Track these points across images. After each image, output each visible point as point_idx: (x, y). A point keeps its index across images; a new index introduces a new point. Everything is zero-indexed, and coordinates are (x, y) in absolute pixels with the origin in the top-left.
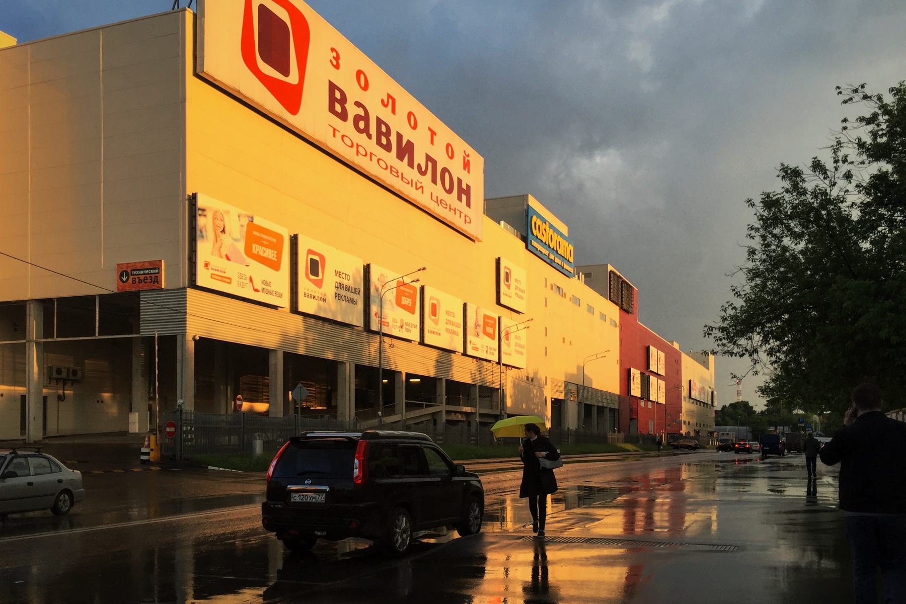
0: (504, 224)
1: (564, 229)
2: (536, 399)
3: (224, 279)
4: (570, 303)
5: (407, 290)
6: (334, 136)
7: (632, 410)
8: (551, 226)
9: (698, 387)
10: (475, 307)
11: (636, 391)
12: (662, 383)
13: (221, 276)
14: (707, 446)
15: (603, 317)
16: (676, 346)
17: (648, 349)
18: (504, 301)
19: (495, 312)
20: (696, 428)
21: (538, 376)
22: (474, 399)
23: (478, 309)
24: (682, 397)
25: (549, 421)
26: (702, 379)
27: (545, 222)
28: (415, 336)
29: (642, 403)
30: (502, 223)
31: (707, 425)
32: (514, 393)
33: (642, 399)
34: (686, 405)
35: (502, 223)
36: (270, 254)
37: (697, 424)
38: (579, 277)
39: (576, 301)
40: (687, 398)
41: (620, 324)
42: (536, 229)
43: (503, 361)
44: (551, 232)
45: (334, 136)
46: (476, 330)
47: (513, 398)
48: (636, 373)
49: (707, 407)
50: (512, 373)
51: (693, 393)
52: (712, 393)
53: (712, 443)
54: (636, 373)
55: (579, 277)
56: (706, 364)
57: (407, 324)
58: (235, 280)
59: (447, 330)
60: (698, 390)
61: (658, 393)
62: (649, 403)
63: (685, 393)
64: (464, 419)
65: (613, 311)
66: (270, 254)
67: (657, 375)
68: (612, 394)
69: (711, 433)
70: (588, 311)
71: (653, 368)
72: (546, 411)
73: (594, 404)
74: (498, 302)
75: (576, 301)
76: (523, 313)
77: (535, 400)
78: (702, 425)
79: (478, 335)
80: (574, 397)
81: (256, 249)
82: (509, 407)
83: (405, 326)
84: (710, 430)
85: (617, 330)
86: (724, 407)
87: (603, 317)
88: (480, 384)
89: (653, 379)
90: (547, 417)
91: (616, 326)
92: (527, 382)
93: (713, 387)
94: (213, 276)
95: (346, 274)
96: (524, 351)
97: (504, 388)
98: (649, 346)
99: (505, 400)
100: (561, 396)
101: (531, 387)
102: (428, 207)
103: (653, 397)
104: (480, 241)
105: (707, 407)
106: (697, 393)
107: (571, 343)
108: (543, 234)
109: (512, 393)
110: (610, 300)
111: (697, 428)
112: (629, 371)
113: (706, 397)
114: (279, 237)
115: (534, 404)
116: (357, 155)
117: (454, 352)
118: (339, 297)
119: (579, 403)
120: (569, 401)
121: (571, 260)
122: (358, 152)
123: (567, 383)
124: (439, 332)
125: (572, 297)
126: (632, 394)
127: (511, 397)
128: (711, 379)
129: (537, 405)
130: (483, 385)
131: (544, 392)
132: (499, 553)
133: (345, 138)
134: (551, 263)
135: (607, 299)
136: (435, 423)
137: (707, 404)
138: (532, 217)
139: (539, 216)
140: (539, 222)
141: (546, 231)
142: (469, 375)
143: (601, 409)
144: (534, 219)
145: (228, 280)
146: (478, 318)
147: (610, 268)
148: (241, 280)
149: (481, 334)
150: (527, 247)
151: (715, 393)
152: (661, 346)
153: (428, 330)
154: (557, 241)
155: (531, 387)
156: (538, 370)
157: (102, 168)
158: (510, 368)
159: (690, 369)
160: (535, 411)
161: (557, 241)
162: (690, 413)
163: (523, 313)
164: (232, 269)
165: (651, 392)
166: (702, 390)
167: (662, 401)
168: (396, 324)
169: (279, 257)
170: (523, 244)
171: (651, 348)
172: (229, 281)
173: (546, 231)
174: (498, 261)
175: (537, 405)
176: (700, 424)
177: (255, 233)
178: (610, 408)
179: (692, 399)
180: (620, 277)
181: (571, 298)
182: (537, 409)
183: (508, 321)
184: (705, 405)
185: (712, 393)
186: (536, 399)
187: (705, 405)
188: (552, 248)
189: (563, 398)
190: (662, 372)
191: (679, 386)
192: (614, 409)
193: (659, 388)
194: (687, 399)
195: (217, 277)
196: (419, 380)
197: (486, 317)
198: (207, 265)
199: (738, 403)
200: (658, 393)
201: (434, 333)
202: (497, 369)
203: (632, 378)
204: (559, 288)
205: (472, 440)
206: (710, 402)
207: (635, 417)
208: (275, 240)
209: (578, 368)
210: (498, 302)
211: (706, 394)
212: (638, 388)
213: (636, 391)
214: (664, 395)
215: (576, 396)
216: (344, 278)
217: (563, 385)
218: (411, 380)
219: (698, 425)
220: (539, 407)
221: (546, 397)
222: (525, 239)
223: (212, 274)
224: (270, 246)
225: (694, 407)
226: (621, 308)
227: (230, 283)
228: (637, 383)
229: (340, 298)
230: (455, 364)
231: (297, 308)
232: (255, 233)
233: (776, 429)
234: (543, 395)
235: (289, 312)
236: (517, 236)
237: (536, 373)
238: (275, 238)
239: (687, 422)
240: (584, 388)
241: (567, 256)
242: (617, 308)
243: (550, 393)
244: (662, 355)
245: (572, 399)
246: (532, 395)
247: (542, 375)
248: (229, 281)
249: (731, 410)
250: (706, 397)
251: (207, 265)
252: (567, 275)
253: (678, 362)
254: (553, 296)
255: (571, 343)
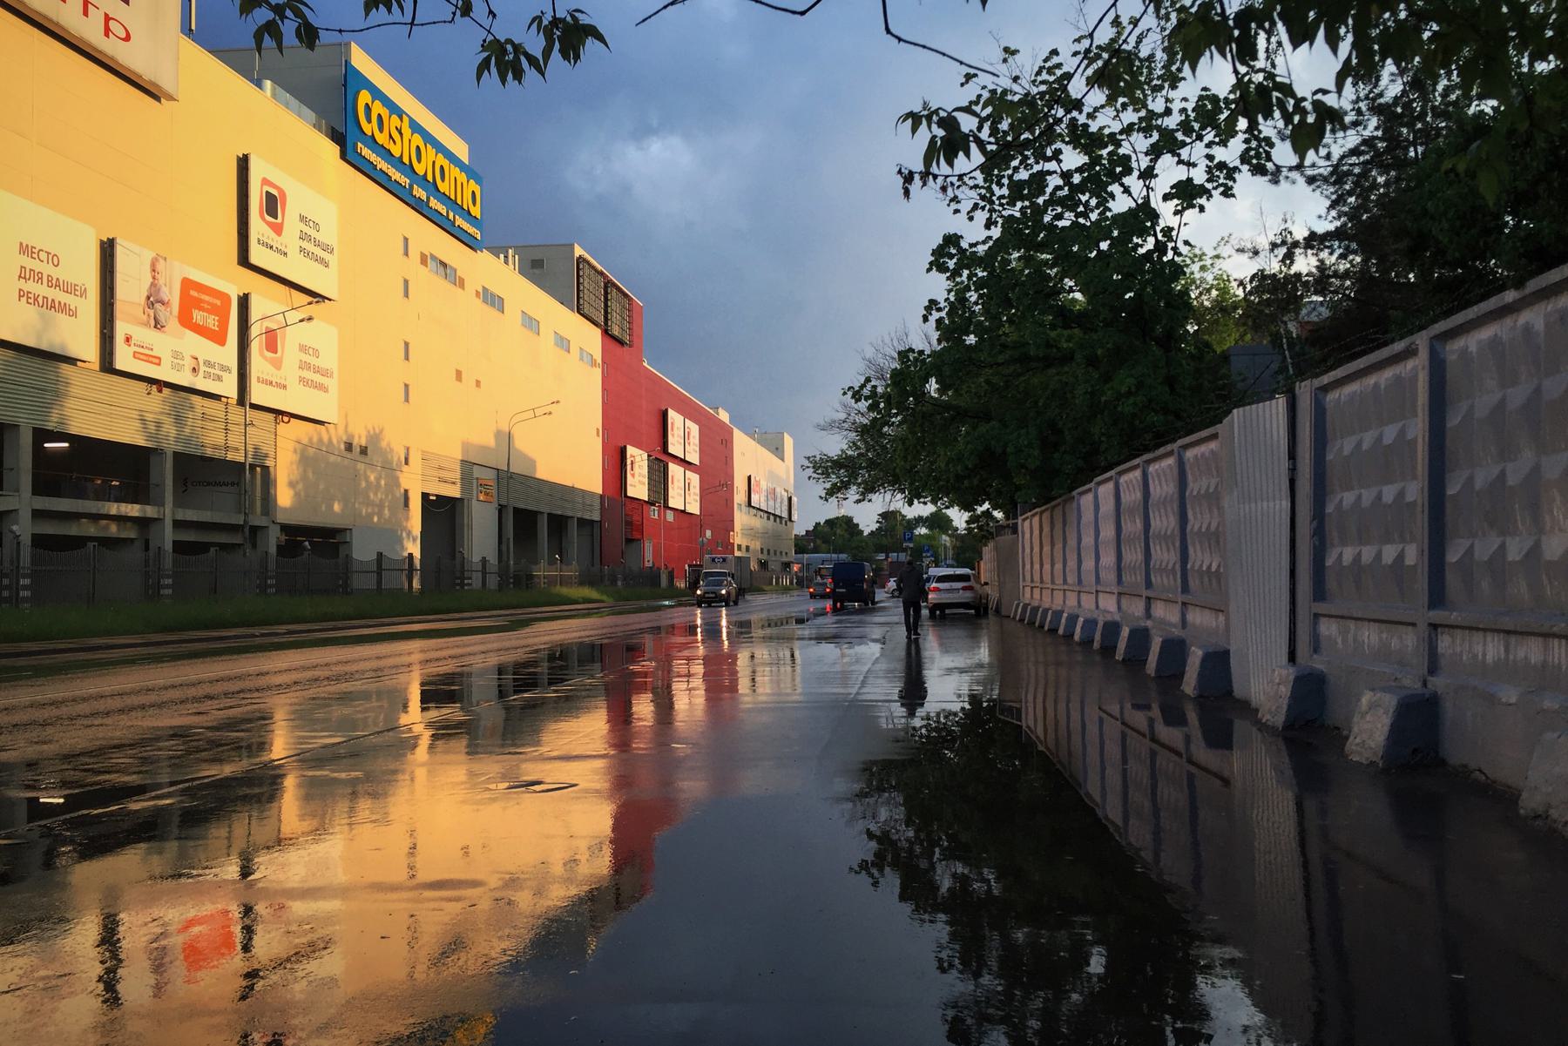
0: (273, 90)
1: (461, 149)
2: (376, 494)
3: (151, 359)
4: (479, 302)
5: (207, 298)
6: (86, 13)
7: (629, 524)
8: (416, 127)
9: (764, 488)
10: (149, 255)
11: (638, 487)
12: (694, 479)
13: (147, 355)
14: (766, 588)
15: (563, 343)
16: (724, 416)
17: (665, 415)
18: (257, 256)
19: (233, 283)
20: (760, 556)
21: (384, 444)
22: (160, 486)
23: (160, 266)
24: (736, 506)
25: (414, 540)
26: (772, 476)
27: (400, 114)
28: (229, 388)
29: (654, 513)
30: (268, 84)
31: (781, 553)
32: (304, 478)
33: (651, 503)
34: (742, 519)
35: (268, 84)
36: (212, 322)
37: (762, 549)
38: (506, 257)
39: (493, 300)
40: (743, 507)
41: (603, 362)
42: (369, 121)
43: (258, 395)
44: (417, 140)
45: (86, 13)
46: (151, 312)
47: (300, 486)
48: (638, 458)
49: (781, 523)
50: (291, 433)
51: (754, 497)
52: (790, 499)
53: (777, 583)
54: (638, 458)
55: (506, 257)
56: (778, 451)
57: (208, 363)
58: (167, 360)
59: (302, 380)
60: (764, 493)
61: (685, 493)
62: (668, 512)
63: (739, 497)
64: (133, 535)
65: (591, 338)
66: (212, 322)
67: (684, 462)
68: (593, 494)
69: (787, 565)
70: (524, 325)
71: (675, 448)
72: (407, 519)
73: (542, 510)
74: (244, 260)
75: (493, 300)
76: (330, 300)
77: (372, 495)
78: (772, 552)
79: (158, 325)
80: (487, 494)
81: (198, 316)
82: (285, 509)
83: (203, 368)
84: (785, 559)
85: (598, 373)
86: (818, 524)
87: (563, 343)
88: (180, 448)
89: (675, 470)
90: (409, 533)
91: (593, 363)
92: (348, 455)
93: (791, 490)
94: (137, 355)
95: (48, 253)
96: (332, 383)
97: (269, 463)
98: (667, 410)
99: (272, 491)
100: (454, 491)
101: (361, 466)
102: (55, 19)
103: (675, 501)
104: (171, 98)
105: (781, 523)
106: (763, 499)
107: (478, 383)
108: (391, 137)
109: (296, 476)
110: (578, 312)
111: (764, 557)
112: (623, 453)
113: (778, 505)
114: (225, 297)
115: (369, 503)
116: (107, 35)
117: (72, 361)
118: (28, 298)
119: (501, 509)
120: (474, 502)
121: (476, 211)
122: (107, 31)
123: (467, 466)
124: (283, 382)
125: (481, 290)
126: (629, 494)
127: (292, 485)
128: (788, 477)
129: (381, 506)
130: (192, 451)
131: (401, 480)
132: (578, 718)
133: (124, 36)
134: (419, 207)
135: (573, 310)
136: (147, 548)
137: (781, 517)
138: (357, 93)
139: (377, 94)
140: (378, 108)
141: (401, 134)
142: (138, 424)
143: (559, 523)
144: (364, 97)
145: (157, 361)
146: (161, 281)
147: (578, 251)
148: (176, 361)
149: (173, 324)
150: (343, 156)
151: (794, 499)
152: (690, 411)
153: (258, 378)
154: (434, 162)
155: (361, 466)
156: (381, 431)
157: (1039, 615)
158: (286, 419)
159: (748, 456)
160: (372, 519)
161: (434, 162)
162: (750, 532)
163: (330, 300)
164: (161, 343)
165: (671, 492)
166: (772, 493)
167: (694, 508)
168: (181, 362)
169: (224, 324)
170: (335, 149)
171: (671, 413)
172: (157, 361)
173: (401, 134)
174: (243, 164)
175: (381, 506)
176: (769, 551)
177: (194, 293)
178: (579, 520)
179: (754, 508)
180: (601, 273)
181: (477, 292)
182: (380, 515)
183: (267, 304)
184: (778, 519)
185: (790, 499)
186: (376, 494)
187: (778, 519)
188: (422, 173)
189: (458, 495)
190: (694, 458)
191: (729, 486)
192: (592, 522)
193: (687, 487)
194: (743, 507)
195: (141, 357)
196: (66, 445)
197: (187, 284)
198: (128, 340)
199: (837, 518)
200: (685, 493)
201: (271, 383)
202: (236, 414)
203: (629, 462)
204: (444, 265)
205: (168, 586)
206: (785, 515)
207: (639, 537)
208: (218, 303)
209: (498, 434)
210: (244, 260)
211: (779, 500)
212: (642, 483)
213: (638, 487)
214: (698, 498)
215: (494, 492)
216: (45, 261)
217: (458, 467)
218: (46, 445)
219: (765, 552)
220: (386, 511)
221: (406, 491)
222: (338, 137)
223: (135, 352)
224: (213, 310)
225: (758, 523)
226: (606, 332)
227: (159, 364)
228: (695, 494)
229: (31, 301)
230: (74, 390)
231: (111, 362)
232: (194, 293)
233: (887, 557)
234: (398, 485)
235: (98, 369)
236: (317, 126)
237: (375, 438)
238: (217, 298)
239: (744, 547)
240: (511, 476)
241: (467, 202)
242: (596, 333)
243: (416, 483)
244: (694, 429)
245: (481, 498)
246: (363, 484)
247: (395, 442)
248: (157, 361)
249: (827, 529)
250: (778, 505)
251: (128, 340)
252: (470, 243)
253: (727, 443)
254: (424, 278)
255: (478, 383)
